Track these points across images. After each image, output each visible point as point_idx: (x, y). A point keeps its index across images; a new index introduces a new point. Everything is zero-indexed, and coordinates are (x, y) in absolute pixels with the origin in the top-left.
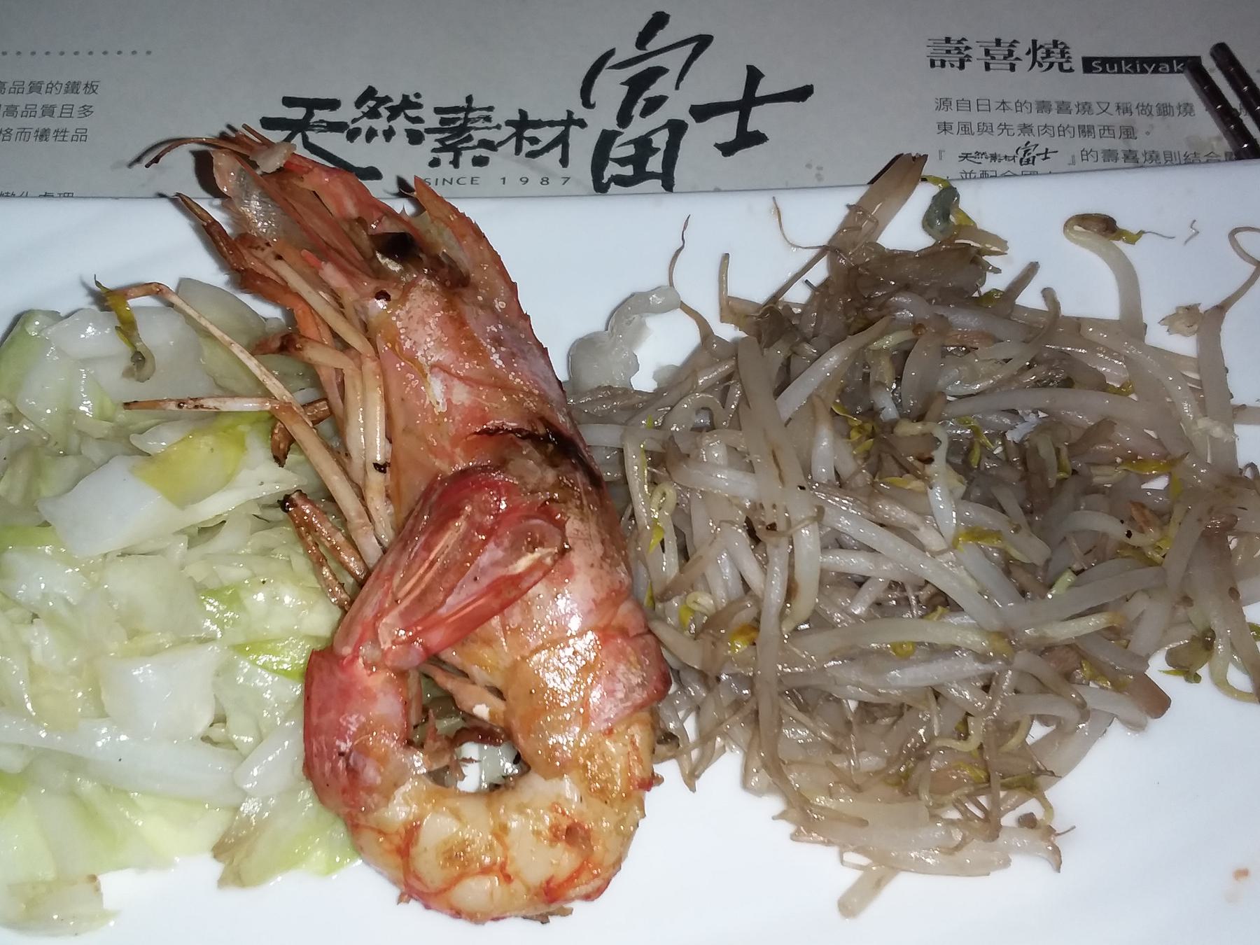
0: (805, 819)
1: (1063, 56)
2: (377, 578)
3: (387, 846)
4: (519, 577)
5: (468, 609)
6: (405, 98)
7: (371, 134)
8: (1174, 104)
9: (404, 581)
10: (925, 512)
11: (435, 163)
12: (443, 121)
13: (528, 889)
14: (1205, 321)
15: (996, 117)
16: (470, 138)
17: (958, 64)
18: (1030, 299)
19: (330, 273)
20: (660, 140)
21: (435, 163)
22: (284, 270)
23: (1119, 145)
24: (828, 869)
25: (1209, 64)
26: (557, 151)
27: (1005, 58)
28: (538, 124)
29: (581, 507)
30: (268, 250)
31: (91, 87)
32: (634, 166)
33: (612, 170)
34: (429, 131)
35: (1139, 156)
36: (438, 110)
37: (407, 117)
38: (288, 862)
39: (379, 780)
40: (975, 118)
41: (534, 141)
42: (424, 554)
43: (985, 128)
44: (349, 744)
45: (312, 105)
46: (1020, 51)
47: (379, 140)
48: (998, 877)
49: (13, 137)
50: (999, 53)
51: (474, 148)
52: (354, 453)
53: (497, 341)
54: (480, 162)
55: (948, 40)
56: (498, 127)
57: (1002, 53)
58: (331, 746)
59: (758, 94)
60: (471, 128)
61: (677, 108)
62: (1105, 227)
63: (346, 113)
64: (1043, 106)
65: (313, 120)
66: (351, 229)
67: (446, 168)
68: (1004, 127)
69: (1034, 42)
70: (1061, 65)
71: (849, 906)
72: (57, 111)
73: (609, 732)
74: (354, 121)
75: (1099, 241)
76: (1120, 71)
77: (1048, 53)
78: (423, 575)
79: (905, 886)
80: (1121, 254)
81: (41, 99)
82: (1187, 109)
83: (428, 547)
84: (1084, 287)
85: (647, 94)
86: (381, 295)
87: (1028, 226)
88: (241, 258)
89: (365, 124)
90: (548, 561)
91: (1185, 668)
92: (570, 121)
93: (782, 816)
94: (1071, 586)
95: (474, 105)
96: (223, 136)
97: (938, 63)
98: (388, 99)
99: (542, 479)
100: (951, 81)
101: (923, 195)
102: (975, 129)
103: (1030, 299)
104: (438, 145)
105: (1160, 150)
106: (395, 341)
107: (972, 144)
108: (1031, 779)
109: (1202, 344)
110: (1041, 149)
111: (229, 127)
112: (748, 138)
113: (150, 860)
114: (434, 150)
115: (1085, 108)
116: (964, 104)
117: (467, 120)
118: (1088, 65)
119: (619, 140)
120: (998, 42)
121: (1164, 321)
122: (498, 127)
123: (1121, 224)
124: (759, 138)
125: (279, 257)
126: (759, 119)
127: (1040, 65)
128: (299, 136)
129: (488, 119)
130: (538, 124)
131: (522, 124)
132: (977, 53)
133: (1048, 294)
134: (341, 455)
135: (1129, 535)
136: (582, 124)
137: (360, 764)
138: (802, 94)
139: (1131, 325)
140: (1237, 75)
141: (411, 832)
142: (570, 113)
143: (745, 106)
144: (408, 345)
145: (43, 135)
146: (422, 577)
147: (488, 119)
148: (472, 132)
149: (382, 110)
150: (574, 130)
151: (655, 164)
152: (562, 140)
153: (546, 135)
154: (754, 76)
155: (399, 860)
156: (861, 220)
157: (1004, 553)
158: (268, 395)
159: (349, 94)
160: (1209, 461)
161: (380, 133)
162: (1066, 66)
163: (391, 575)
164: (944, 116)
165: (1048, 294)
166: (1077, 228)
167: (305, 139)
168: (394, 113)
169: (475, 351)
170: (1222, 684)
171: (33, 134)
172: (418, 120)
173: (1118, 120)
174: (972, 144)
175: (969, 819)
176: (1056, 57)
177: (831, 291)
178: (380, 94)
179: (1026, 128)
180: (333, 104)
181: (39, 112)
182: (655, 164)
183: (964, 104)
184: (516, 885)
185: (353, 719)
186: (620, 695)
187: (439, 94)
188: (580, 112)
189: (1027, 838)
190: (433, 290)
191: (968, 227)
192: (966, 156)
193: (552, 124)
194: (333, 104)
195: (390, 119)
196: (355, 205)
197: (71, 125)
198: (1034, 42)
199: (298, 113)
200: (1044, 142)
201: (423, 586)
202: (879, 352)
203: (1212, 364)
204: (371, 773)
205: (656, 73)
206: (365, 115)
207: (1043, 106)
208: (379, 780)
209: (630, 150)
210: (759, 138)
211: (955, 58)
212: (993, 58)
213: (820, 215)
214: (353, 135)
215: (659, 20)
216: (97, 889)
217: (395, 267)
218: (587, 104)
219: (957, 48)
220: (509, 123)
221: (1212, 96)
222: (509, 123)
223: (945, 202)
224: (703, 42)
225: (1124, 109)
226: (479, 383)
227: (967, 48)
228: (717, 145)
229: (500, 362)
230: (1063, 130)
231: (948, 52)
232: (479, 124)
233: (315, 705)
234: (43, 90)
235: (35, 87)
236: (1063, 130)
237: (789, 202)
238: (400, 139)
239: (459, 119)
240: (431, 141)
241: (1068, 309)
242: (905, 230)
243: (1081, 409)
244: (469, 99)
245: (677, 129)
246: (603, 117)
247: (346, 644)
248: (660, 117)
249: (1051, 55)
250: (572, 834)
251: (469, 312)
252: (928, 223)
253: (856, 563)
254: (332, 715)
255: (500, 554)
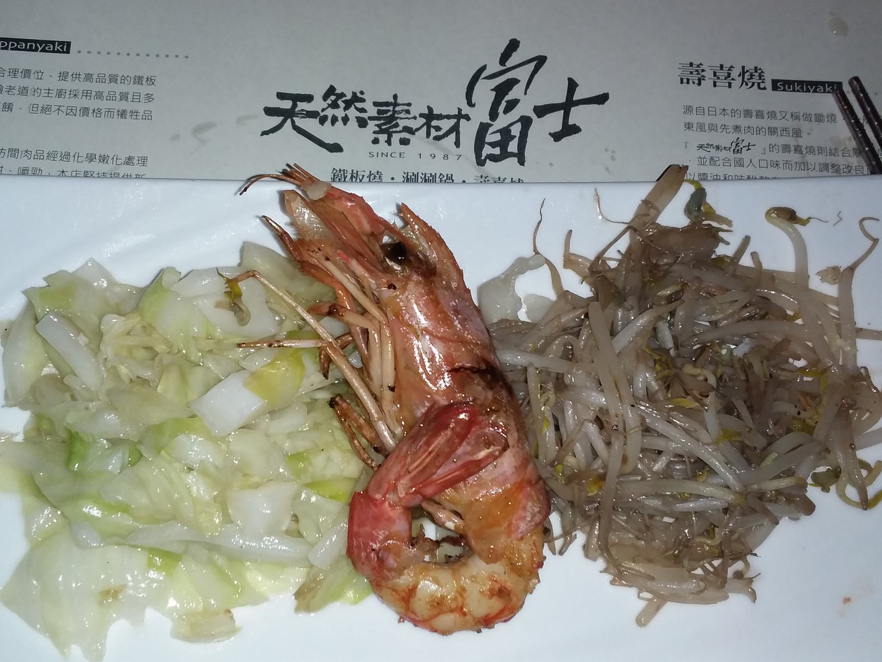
0: (620, 576)
1: (760, 79)
2: (397, 457)
3: (397, 597)
4: (480, 461)
5: (450, 476)
6: (354, 94)
7: (334, 120)
8: (825, 114)
9: (413, 461)
10: (703, 423)
11: (376, 141)
12: (379, 112)
13: (474, 618)
14: (843, 276)
15: (719, 120)
16: (397, 125)
17: (697, 82)
18: (746, 261)
19: (354, 265)
20: (516, 130)
21: (376, 141)
22: (329, 266)
23: (791, 141)
24: (630, 600)
25: (846, 88)
26: (453, 136)
27: (726, 79)
28: (440, 117)
29: (505, 412)
30: (320, 254)
31: (151, 81)
32: (500, 148)
33: (487, 150)
34: (371, 118)
35: (803, 149)
36: (376, 104)
37: (357, 108)
38: (335, 596)
39: (396, 565)
40: (706, 120)
41: (438, 129)
42: (426, 447)
43: (713, 128)
44: (378, 545)
45: (296, 98)
46: (735, 73)
47: (340, 123)
48: (721, 606)
49: (103, 115)
50: (722, 74)
51: (400, 132)
52: (375, 379)
53: (457, 312)
54: (404, 142)
55: (691, 64)
56: (415, 118)
57: (723, 75)
58: (366, 545)
59: (575, 98)
60: (398, 118)
61: (525, 109)
62: (787, 216)
63: (317, 105)
64: (748, 113)
65: (297, 109)
66: (369, 240)
67: (382, 146)
68: (724, 127)
69: (743, 67)
70: (759, 84)
71: (642, 620)
72: (130, 97)
73: (522, 538)
74: (323, 110)
75: (785, 224)
76: (794, 90)
77: (752, 75)
78: (424, 459)
79: (671, 609)
80: (796, 230)
81: (119, 88)
82: (832, 118)
83: (428, 444)
84: (775, 252)
85: (507, 98)
86: (391, 286)
87: (745, 215)
88: (300, 254)
89: (330, 112)
90: (497, 453)
91: (823, 483)
92: (460, 116)
93: (606, 571)
94: (776, 459)
95: (399, 101)
96: (285, 172)
97: (685, 81)
98: (342, 95)
99: (486, 398)
100: (693, 94)
101: (686, 191)
102: (707, 128)
103: (746, 261)
104: (377, 129)
105: (815, 145)
106: (398, 314)
107: (706, 138)
108: (743, 553)
109: (840, 291)
110: (745, 143)
111: (288, 165)
112: (569, 130)
113: (258, 599)
114: (375, 132)
115: (772, 115)
116: (700, 110)
117: (394, 112)
118: (776, 85)
119: (491, 130)
120: (722, 67)
121: (819, 273)
122: (415, 118)
123: (799, 214)
124: (575, 129)
125: (327, 259)
126: (577, 115)
127: (747, 84)
128: (289, 120)
129: (408, 112)
130: (440, 117)
131: (430, 116)
132: (709, 74)
133: (754, 255)
134: (364, 371)
135: (799, 413)
136: (467, 118)
137: (385, 556)
138: (601, 99)
139: (802, 274)
140: (865, 101)
141: (412, 591)
142: (460, 110)
143: (567, 106)
144: (407, 316)
145: (122, 114)
146: (424, 460)
147: (408, 112)
148: (398, 121)
149: (340, 102)
150: (463, 121)
151: (513, 147)
152: (455, 129)
153: (446, 125)
154: (572, 85)
155: (403, 604)
156: (650, 207)
157: (742, 442)
158: (319, 337)
159: (318, 92)
160: (841, 363)
161: (340, 119)
162: (762, 86)
163: (406, 457)
164: (689, 118)
165: (754, 255)
166: (774, 215)
167: (293, 122)
168: (348, 104)
169: (446, 321)
170: (842, 496)
171: (116, 113)
172: (363, 110)
173: (791, 124)
174: (706, 138)
175: (708, 574)
176: (756, 79)
177: (633, 257)
178: (338, 91)
179: (737, 128)
180: (309, 98)
181: (118, 98)
182: (513, 147)
183: (700, 110)
184: (468, 617)
185: (381, 533)
186: (529, 519)
187: (377, 92)
188: (466, 110)
189: (738, 583)
190: (420, 283)
191: (711, 214)
192: (701, 147)
193: (448, 117)
194: (309, 98)
195: (346, 109)
196: (368, 223)
197: (141, 107)
198: (743, 67)
199: (287, 104)
200: (748, 138)
201: (424, 465)
202: (660, 298)
203: (845, 300)
204: (391, 561)
205: (514, 82)
206: (330, 106)
207: (748, 113)
208: (396, 565)
209: (497, 137)
210: (575, 129)
211: (695, 77)
212: (718, 78)
213: (625, 203)
214: (323, 120)
215: (513, 45)
216: (232, 618)
217: (397, 267)
218: (470, 104)
219: (697, 71)
220: (421, 115)
221: (848, 112)
222: (421, 115)
223: (699, 196)
224: (541, 61)
225: (795, 116)
226: (450, 340)
227: (703, 71)
228: (550, 134)
229: (459, 326)
230: (759, 130)
231: (691, 73)
232: (402, 115)
233: (356, 521)
234: (119, 81)
235: (113, 79)
236: (759, 130)
237: (603, 191)
238: (353, 123)
239: (389, 111)
240: (372, 126)
241: (767, 265)
242: (674, 215)
243: (775, 332)
244: (395, 97)
245: (526, 122)
246: (480, 114)
247: (378, 492)
248: (515, 114)
249: (752, 77)
250: (501, 592)
251: (440, 293)
252: (688, 210)
253: (659, 444)
254: (368, 529)
255: (469, 448)
